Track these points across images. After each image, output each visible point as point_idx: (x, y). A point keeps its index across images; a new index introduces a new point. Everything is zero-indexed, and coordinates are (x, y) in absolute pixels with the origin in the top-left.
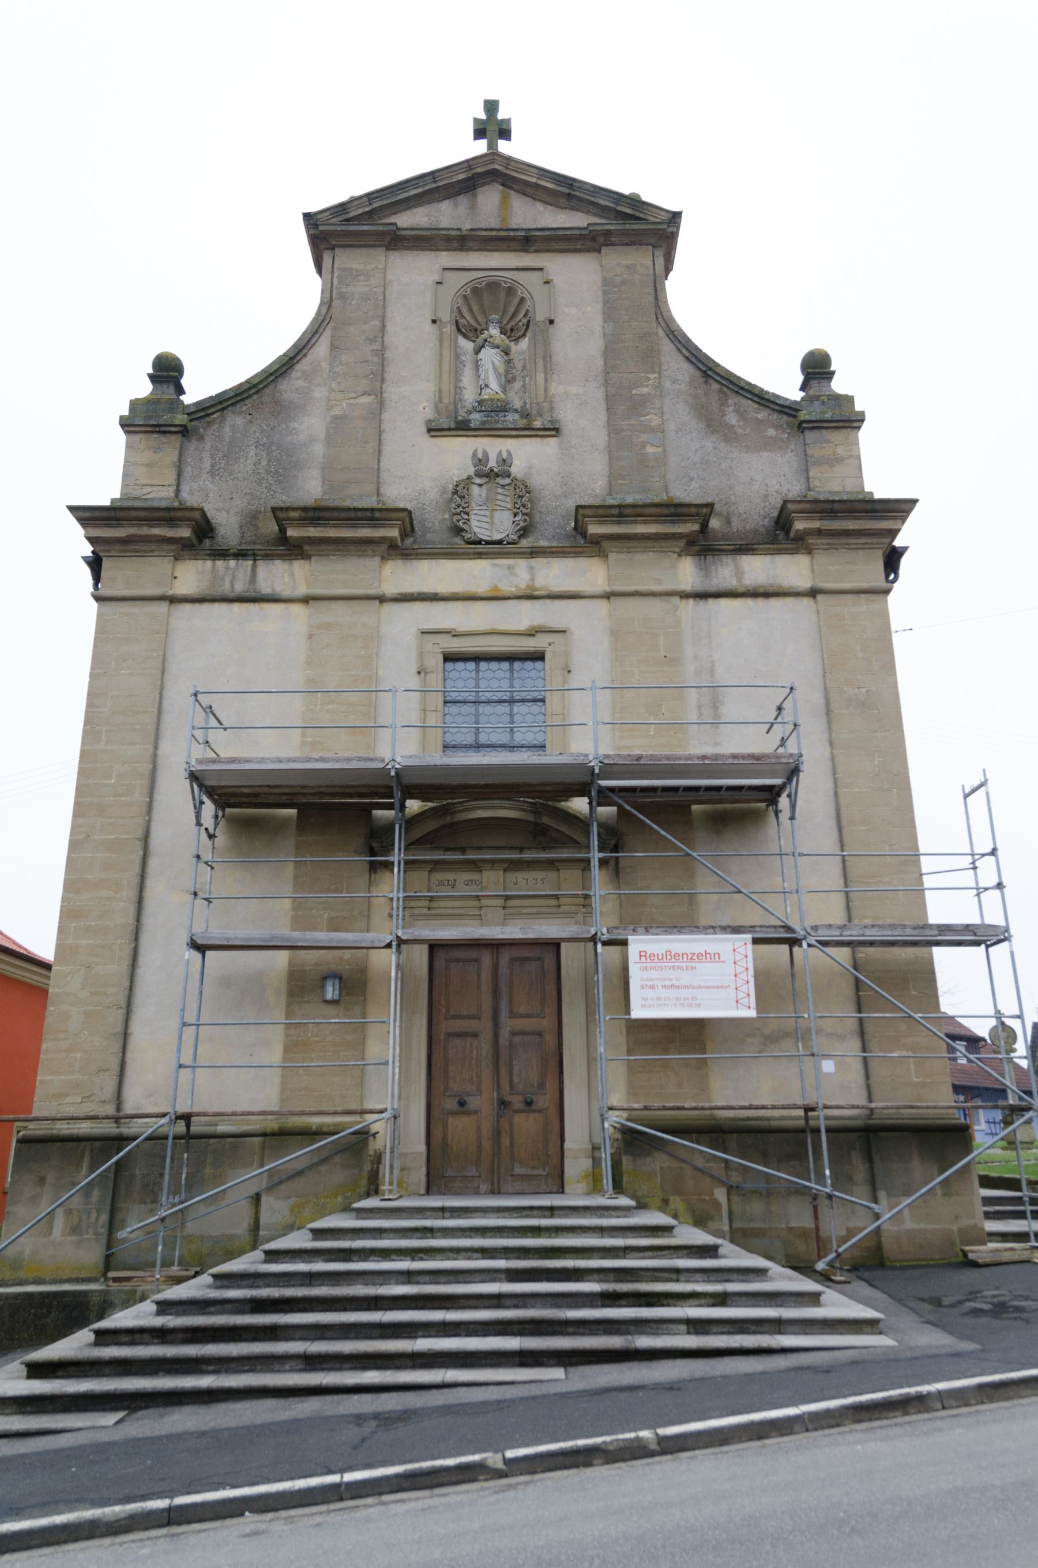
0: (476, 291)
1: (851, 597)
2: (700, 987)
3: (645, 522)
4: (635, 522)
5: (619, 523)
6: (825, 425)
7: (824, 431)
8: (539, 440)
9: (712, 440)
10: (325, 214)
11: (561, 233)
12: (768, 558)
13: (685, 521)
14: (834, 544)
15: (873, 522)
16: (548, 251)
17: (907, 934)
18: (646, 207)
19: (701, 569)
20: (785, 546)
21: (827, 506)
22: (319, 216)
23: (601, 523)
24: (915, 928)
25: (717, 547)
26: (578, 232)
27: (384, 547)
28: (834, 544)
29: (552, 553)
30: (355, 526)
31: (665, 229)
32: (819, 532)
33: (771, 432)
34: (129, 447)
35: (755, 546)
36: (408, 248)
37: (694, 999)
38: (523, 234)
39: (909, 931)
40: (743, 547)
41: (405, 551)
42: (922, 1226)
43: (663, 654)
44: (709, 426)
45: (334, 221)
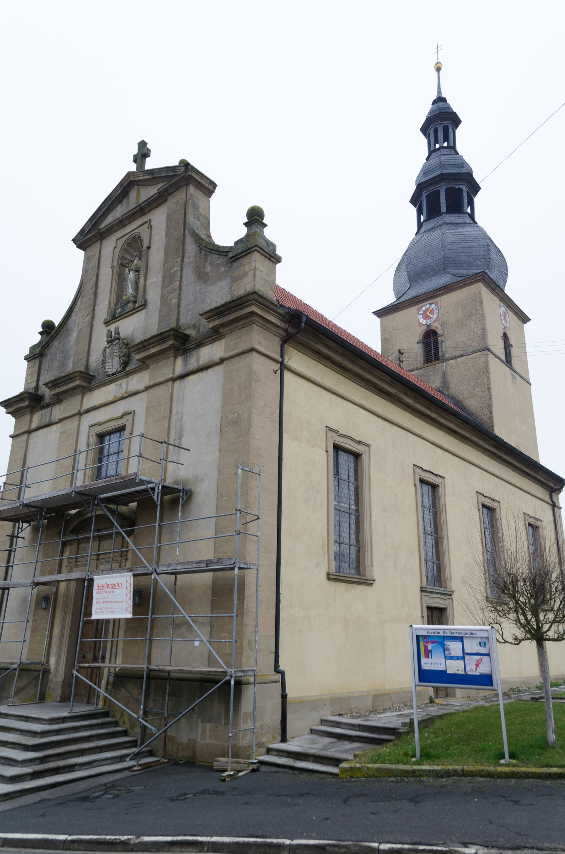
0: (129, 244)
1: (237, 358)
2: (115, 602)
3: (154, 347)
4: (150, 348)
5: (145, 351)
6: (240, 256)
7: (241, 260)
8: (139, 313)
9: (199, 284)
10: (78, 237)
11: (150, 200)
12: (210, 346)
13: (167, 341)
14: (232, 329)
15: (241, 311)
16: (152, 210)
17: (194, 567)
18: (176, 168)
19: (184, 362)
20: (215, 337)
21: (218, 311)
22: (76, 239)
23: (139, 353)
24: (197, 563)
25: (188, 348)
26: (156, 196)
27: (80, 390)
28: (232, 329)
29: (133, 372)
30: (67, 384)
31: (184, 176)
32: (223, 325)
33: (222, 269)
34: (28, 368)
35: (203, 342)
36: (108, 236)
37: (112, 608)
38: (138, 208)
39: (195, 565)
40: (198, 344)
41: (89, 388)
42: (213, 742)
43: (162, 415)
44: (199, 277)
45: (81, 238)
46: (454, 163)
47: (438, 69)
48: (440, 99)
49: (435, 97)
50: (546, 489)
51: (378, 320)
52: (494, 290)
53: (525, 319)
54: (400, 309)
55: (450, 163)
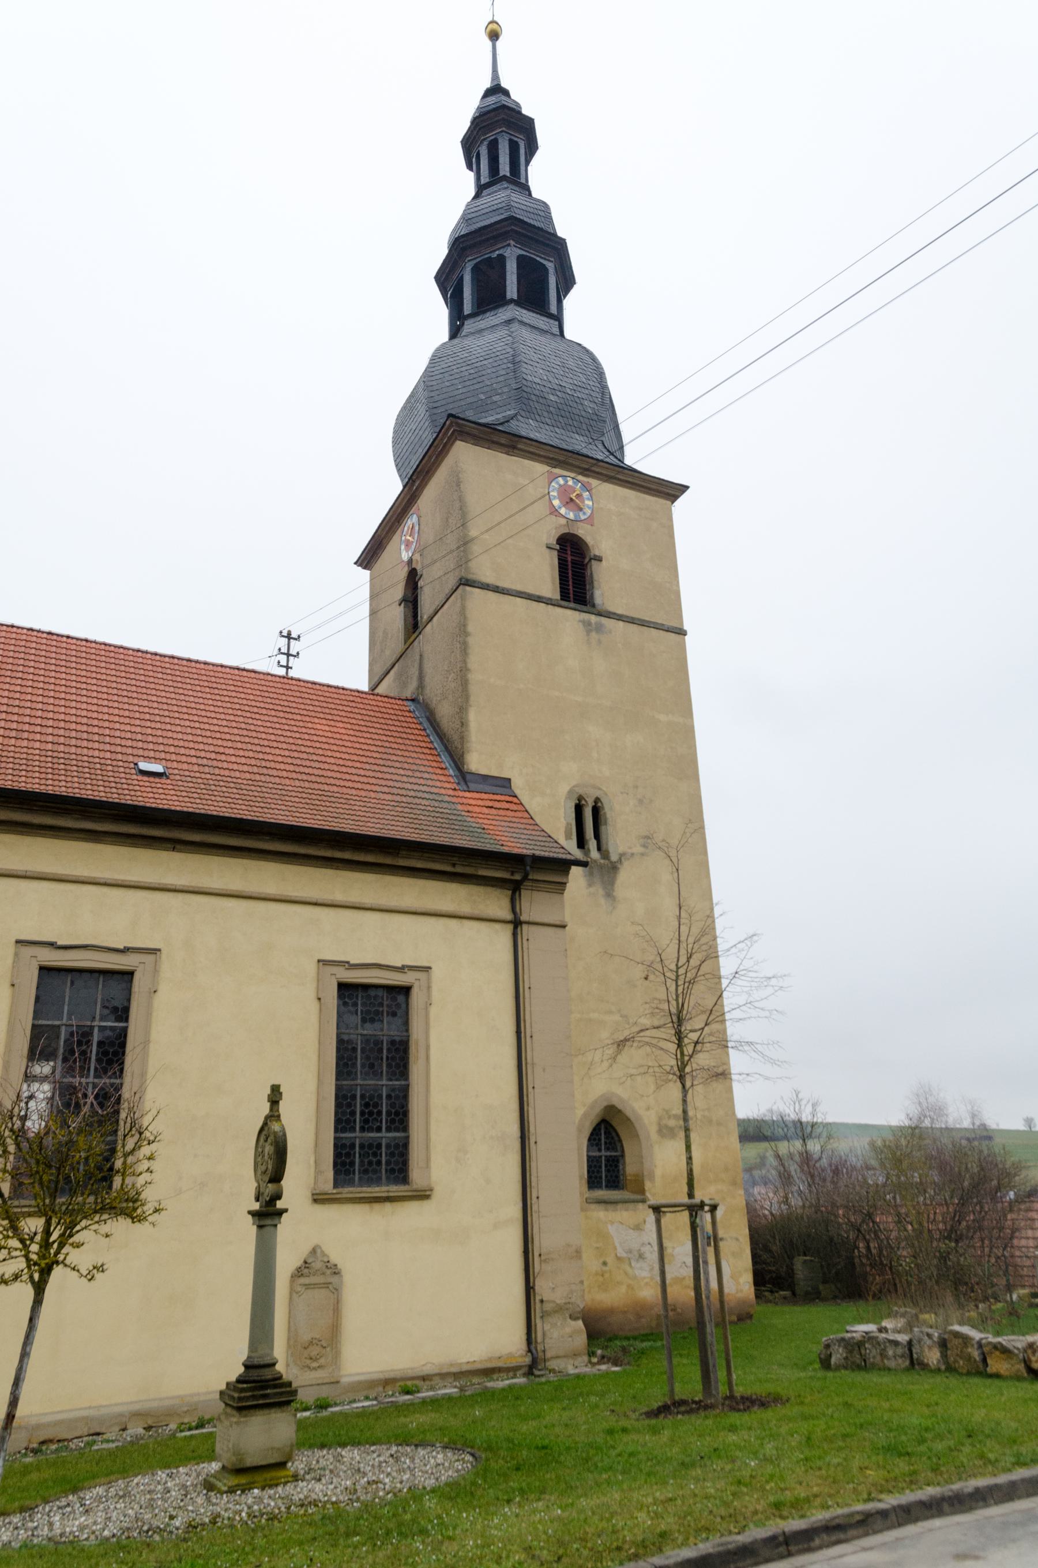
46: (490, 209)
47: (494, 36)
48: (496, 89)
49: (488, 84)
50: (493, 886)
52: (514, 447)
54: (384, 541)
55: (483, 212)
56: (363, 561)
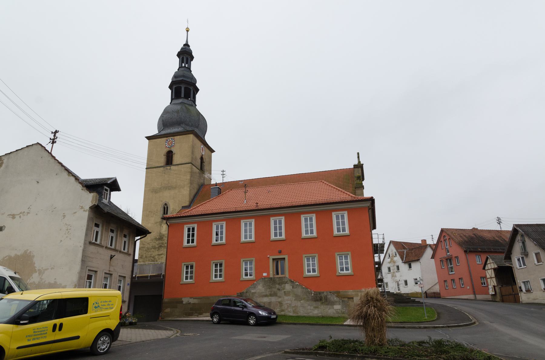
47: (187, 31)
48: (187, 45)
49: (185, 43)
51: (148, 141)
53: (213, 151)
56: (433, 257)
